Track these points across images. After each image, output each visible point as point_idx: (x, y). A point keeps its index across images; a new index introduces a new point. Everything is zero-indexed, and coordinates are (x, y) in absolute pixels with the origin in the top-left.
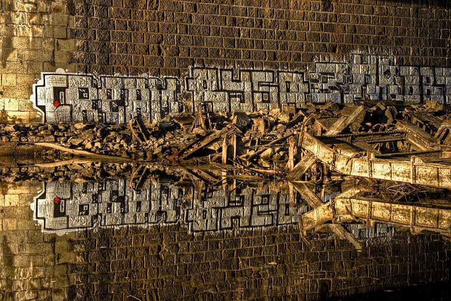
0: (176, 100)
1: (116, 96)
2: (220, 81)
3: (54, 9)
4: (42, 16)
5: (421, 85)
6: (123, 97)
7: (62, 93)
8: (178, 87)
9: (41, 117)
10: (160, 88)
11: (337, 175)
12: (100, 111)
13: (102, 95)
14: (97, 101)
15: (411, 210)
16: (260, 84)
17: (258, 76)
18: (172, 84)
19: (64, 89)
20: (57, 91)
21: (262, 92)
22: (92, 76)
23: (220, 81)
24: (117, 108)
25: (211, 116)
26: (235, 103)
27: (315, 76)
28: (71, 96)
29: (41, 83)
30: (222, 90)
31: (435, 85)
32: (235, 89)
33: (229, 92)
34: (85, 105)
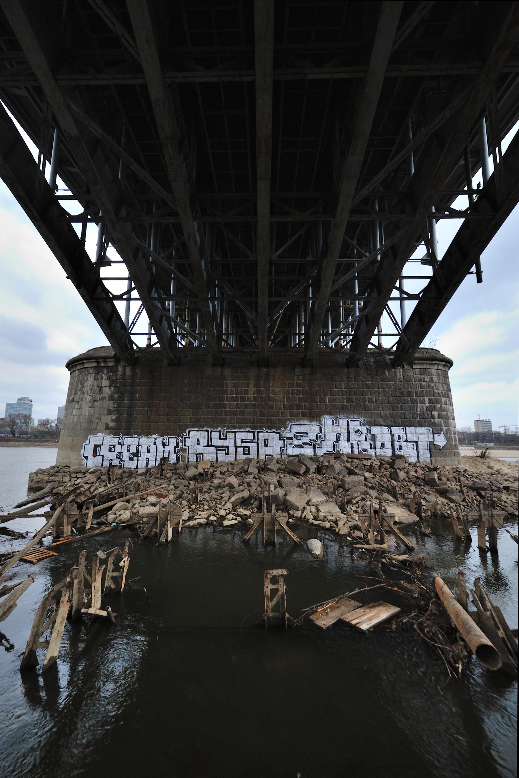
0: (175, 453)
1: (133, 450)
2: (210, 438)
3: (102, 398)
4: (94, 403)
5: (392, 442)
6: (137, 450)
7: (98, 448)
8: (178, 444)
9: (85, 463)
10: (164, 444)
11: (62, 546)
12: (121, 460)
13: (124, 449)
14: (120, 453)
15: (385, 546)
16: (242, 441)
17: (240, 436)
18: (173, 441)
19: (100, 446)
20: (96, 447)
21: (244, 447)
22: (119, 438)
23: (210, 438)
24: (133, 457)
25: (457, 665)
26: (221, 456)
27: (291, 435)
28: (104, 451)
29: (87, 442)
30: (211, 446)
31: (406, 441)
32: (221, 445)
33: (216, 447)
34: (113, 455)
